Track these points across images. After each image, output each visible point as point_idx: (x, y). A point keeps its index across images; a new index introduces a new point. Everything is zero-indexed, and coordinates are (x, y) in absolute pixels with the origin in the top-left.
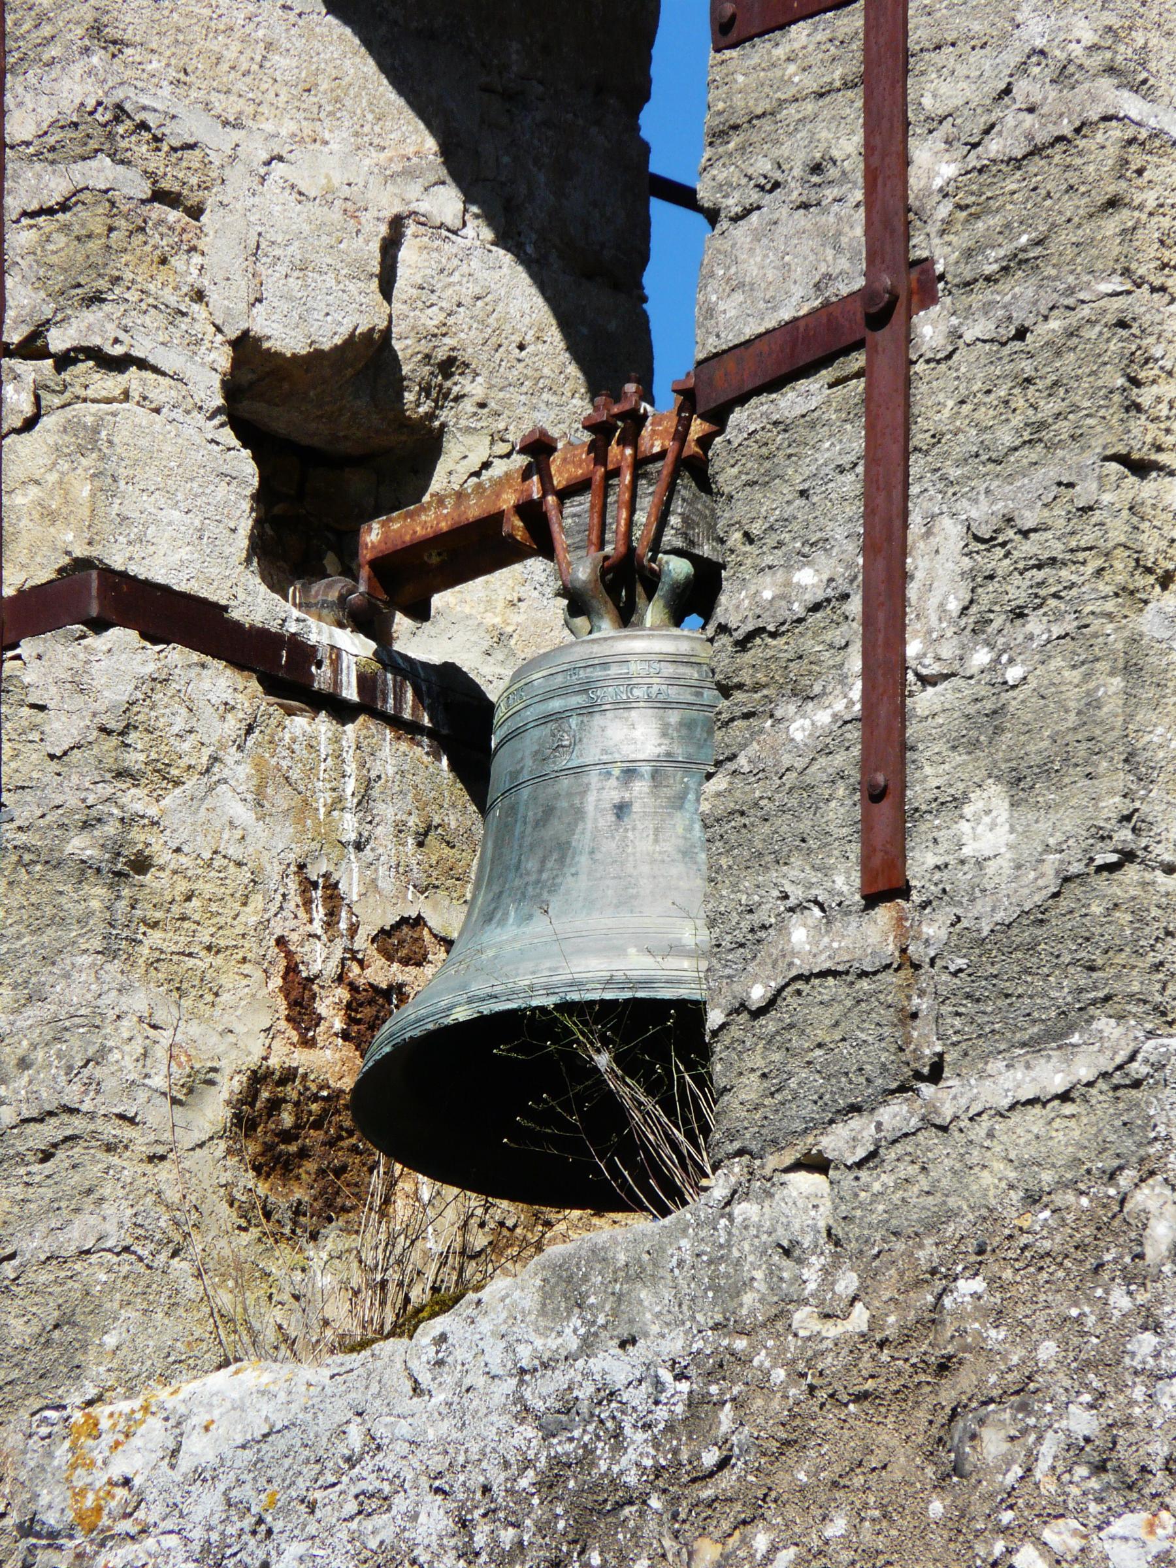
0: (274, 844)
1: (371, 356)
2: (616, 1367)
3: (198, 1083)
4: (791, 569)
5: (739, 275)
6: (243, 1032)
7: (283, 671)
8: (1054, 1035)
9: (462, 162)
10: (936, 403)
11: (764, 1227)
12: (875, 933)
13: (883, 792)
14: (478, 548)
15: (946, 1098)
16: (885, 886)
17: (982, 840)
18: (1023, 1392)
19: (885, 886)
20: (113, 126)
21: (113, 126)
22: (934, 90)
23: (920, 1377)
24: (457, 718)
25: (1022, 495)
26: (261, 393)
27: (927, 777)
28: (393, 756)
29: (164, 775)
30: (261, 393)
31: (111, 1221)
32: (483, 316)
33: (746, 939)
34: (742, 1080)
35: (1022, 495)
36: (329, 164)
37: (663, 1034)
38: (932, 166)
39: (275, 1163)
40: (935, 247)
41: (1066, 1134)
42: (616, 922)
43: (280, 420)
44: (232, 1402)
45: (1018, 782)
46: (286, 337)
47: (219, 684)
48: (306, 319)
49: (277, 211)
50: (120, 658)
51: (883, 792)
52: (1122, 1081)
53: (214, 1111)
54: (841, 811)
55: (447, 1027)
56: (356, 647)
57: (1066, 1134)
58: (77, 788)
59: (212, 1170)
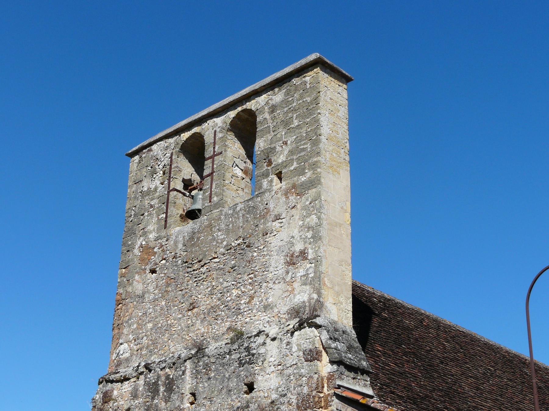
0: (183, 203)
1: (190, 180)
2: (196, 226)
3: (178, 214)
4: (206, 187)
5: (206, 172)
6: (181, 212)
7: (184, 194)
8: (218, 209)
9: (196, 171)
10: (214, 178)
11: (203, 219)
12: (210, 204)
13: (210, 197)
14: (194, 189)
15: (212, 212)
16: (210, 202)
17: (215, 199)
18: (215, 226)
19: (210, 202)
20: (177, 167)
21: (177, 167)
22: (215, 163)
23: (210, 226)
24: (193, 197)
25: (218, 182)
26: (184, 181)
27: (213, 196)
28: (190, 199)
29: (177, 199)
30: (184, 181)
31: (173, 220)
32: (196, 178)
33: (203, 205)
34: (203, 212)
35: (218, 182)
36: (189, 170)
37: (199, 210)
38: (215, 166)
39: (182, 218)
40: (215, 170)
41: (218, 213)
42: (198, 206)
43: (186, 183)
44: (178, 229)
45: (217, 196)
46: (185, 178)
47: (181, 194)
48: (187, 177)
49: (185, 172)
50: (175, 193)
51: (210, 197)
52: (221, 211)
53: (179, 215)
54: (208, 198)
55: (358, 340)
56: (188, 194)
57: (218, 213)
58: (173, 199)
59: (179, 219)
